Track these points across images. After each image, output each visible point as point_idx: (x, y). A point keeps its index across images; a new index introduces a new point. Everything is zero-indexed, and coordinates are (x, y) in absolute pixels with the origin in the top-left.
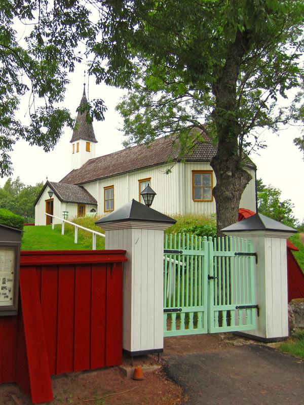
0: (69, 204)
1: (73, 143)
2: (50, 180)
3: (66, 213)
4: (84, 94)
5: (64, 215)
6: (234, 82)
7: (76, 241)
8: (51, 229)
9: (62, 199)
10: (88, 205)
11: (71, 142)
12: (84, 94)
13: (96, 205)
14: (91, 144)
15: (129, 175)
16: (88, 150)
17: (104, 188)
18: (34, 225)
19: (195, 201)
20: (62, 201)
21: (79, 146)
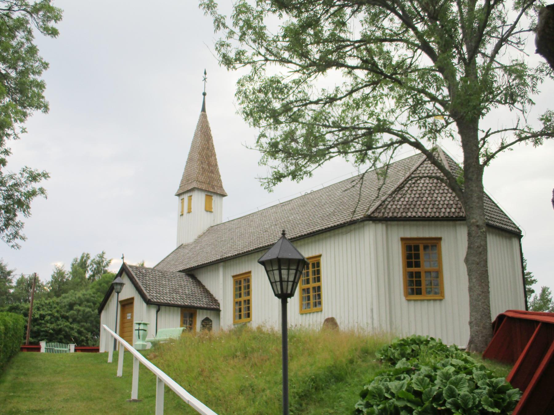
0: (172, 308)
1: (182, 197)
2: (128, 262)
3: (142, 327)
4: (204, 110)
5: (139, 330)
6: (476, 116)
7: (134, 396)
8: (106, 362)
9: (149, 297)
10: (201, 311)
11: (179, 195)
12: (204, 110)
13: (217, 311)
14: (215, 199)
15: (224, 267)
16: (209, 209)
17: (234, 277)
18: (97, 350)
19: (409, 300)
20: (149, 302)
21: (192, 201)
